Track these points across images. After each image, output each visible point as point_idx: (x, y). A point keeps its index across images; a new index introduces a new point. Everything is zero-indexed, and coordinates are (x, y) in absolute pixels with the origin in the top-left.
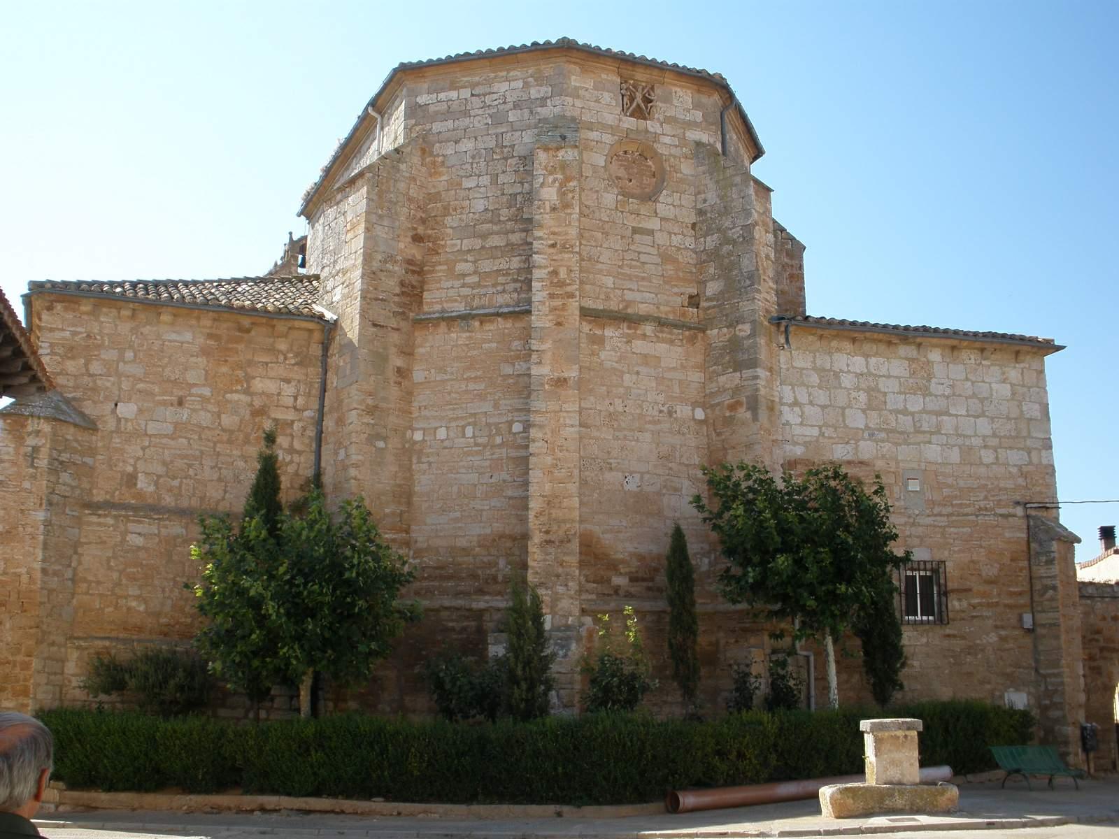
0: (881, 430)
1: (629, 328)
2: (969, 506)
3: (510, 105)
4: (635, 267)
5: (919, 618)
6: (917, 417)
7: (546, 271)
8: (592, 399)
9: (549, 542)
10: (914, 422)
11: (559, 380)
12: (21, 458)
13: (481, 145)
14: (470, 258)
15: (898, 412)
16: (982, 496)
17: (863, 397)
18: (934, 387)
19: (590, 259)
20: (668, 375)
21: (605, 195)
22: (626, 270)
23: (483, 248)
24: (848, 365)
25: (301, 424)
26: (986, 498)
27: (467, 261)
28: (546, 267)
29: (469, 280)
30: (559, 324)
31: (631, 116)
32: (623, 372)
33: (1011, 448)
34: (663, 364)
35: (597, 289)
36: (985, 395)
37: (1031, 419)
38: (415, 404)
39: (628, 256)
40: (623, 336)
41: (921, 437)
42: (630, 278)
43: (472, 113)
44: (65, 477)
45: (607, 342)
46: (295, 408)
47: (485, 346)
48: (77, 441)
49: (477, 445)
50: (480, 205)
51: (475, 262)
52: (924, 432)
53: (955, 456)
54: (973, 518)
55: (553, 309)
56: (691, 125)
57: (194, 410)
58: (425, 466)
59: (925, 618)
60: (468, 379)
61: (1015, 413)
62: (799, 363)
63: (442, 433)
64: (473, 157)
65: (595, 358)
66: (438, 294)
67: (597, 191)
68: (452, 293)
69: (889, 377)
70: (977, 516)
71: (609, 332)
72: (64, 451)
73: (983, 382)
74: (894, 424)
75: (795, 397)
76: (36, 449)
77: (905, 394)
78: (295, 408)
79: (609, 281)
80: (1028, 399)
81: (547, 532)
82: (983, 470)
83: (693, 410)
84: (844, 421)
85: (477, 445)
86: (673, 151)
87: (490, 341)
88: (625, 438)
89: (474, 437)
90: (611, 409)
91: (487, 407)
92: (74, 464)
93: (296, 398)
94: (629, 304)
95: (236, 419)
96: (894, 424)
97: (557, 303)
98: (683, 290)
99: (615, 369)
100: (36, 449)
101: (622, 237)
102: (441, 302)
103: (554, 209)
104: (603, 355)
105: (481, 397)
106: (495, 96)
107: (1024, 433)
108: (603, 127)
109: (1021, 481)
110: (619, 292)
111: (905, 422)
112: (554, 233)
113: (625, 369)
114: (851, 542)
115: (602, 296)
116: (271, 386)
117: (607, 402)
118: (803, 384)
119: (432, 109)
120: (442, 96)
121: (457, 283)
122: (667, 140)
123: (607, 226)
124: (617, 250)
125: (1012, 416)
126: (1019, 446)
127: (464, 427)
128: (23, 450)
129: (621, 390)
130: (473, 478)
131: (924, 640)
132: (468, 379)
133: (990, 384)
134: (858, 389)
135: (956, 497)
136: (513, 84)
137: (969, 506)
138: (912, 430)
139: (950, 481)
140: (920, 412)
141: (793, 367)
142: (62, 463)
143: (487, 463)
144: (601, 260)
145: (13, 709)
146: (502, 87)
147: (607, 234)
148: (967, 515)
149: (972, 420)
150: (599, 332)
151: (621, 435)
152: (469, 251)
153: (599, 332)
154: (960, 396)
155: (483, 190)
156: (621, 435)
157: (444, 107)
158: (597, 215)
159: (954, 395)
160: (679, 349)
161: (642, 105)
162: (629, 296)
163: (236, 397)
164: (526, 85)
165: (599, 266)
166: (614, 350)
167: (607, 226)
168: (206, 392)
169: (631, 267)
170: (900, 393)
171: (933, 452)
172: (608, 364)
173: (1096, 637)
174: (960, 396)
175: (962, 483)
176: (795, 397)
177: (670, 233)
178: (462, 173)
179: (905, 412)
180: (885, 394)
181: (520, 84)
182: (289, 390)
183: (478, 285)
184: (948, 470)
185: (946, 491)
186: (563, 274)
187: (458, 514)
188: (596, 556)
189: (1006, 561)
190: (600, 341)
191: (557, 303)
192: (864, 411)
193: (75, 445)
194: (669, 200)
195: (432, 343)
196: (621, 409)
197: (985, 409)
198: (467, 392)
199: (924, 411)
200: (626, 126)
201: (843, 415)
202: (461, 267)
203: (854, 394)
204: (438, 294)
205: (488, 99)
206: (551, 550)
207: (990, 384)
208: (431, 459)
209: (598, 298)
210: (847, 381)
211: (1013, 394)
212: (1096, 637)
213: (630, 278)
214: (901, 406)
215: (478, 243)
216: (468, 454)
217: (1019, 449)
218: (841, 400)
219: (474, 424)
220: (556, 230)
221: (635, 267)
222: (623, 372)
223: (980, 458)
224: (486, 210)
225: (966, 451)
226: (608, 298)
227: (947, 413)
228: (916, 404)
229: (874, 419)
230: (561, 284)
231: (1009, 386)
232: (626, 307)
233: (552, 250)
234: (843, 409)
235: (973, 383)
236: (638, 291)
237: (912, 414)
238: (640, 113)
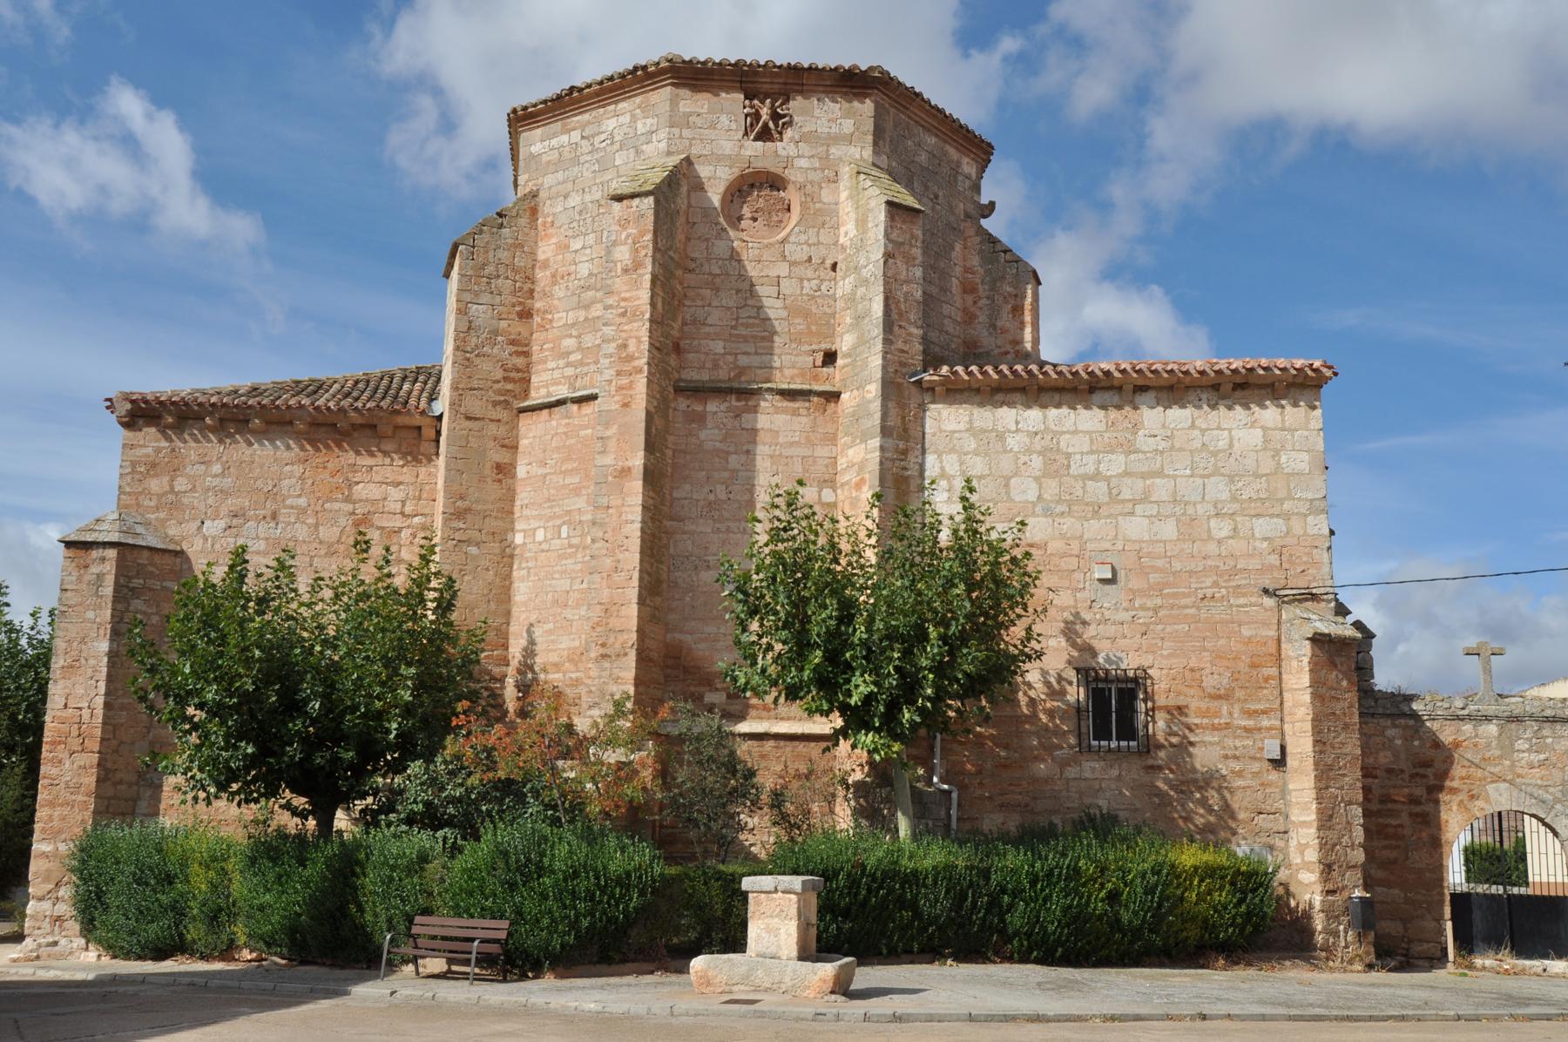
0: (1059, 501)
1: (738, 400)
2: (1185, 595)
3: (617, 146)
4: (753, 325)
5: (1114, 744)
6: (1114, 482)
7: (614, 345)
8: (688, 487)
9: (604, 656)
10: (1110, 490)
11: (623, 470)
12: (84, 587)
13: (588, 198)
14: (574, 333)
15: (1086, 477)
16: (1209, 582)
17: (1037, 462)
18: (1142, 441)
19: (694, 322)
20: (786, 452)
21: (717, 242)
22: (742, 331)
23: (586, 319)
24: (1017, 423)
25: (410, 531)
26: (1216, 584)
27: (571, 336)
28: (613, 340)
29: (572, 358)
30: (626, 405)
31: (755, 140)
32: (728, 453)
33: (1258, 516)
34: (781, 440)
35: (703, 357)
36: (1222, 444)
37: (1292, 474)
38: (518, 503)
39: (744, 313)
40: (729, 410)
41: (1118, 508)
42: (745, 339)
43: (582, 160)
44: (137, 604)
45: (709, 418)
46: (402, 513)
47: (583, 433)
48: (155, 565)
49: (570, 546)
50: (584, 269)
51: (579, 337)
52: (1123, 501)
53: (1169, 530)
54: (1192, 611)
55: (620, 388)
56: (836, 139)
57: (289, 524)
58: (524, 572)
59: (1123, 743)
60: (565, 473)
61: (1267, 466)
62: (950, 426)
63: (540, 535)
64: (580, 213)
65: (693, 440)
66: (545, 376)
67: (707, 240)
68: (557, 374)
69: (1076, 432)
70: (1198, 608)
71: (712, 406)
72: (138, 575)
73: (1219, 428)
74: (1080, 493)
75: (942, 468)
76: (100, 577)
77: (1097, 452)
78: (402, 513)
79: (718, 346)
80: (1289, 447)
81: (603, 645)
82: (1212, 548)
83: (820, 493)
84: (1008, 493)
85: (570, 546)
86: (812, 176)
87: (587, 427)
88: (728, 530)
89: (569, 537)
90: (712, 497)
91: (581, 503)
92: (151, 590)
93: (403, 503)
94: (742, 371)
95: (336, 530)
96: (1080, 493)
97: (624, 381)
98: (814, 347)
99: (719, 450)
100: (100, 577)
101: (738, 291)
102: (547, 386)
103: (626, 271)
104: (703, 435)
105: (576, 491)
106: (603, 137)
107: (1282, 494)
108: (718, 159)
109: (1273, 559)
110: (730, 358)
111: (1098, 490)
112: (625, 300)
113: (732, 449)
114: (819, 653)
115: (709, 365)
116: (373, 491)
117: (706, 490)
118: (952, 450)
119: (545, 158)
120: (554, 142)
121: (561, 363)
122: (803, 163)
123: (718, 280)
124: (729, 308)
125: (1263, 470)
126: (1271, 511)
127: (560, 527)
128: (87, 578)
129: (726, 474)
130: (564, 584)
131: (1115, 772)
132: (565, 473)
133: (1230, 430)
134: (1029, 451)
135: (1167, 585)
136: (621, 119)
137: (1185, 595)
138: (1107, 499)
139: (1160, 563)
140: (1119, 475)
141: (941, 431)
142: (132, 589)
143: (578, 567)
144: (709, 321)
145: (744, 875)
146: (610, 124)
147: (718, 290)
148: (1187, 607)
149: (1199, 481)
150: (699, 408)
151: (722, 527)
152: (573, 325)
153: (699, 408)
154: (1181, 450)
155: (588, 251)
156: (722, 527)
157: (554, 155)
158: (706, 268)
159: (1172, 448)
160: (804, 420)
161: (771, 125)
162: (743, 361)
163: (336, 506)
164: (634, 119)
165: (707, 329)
166: (718, 427)
167: (718, 280)
168: (302, 501)
169: (747, 326)
170: (1092, 452)
171: (1136, 527)
172: (709, 445)
173: (1421, 771)
174: (1181, 450)
175: (1177, 565)
176: (942, 468)
177: (802, 280)
178: (570, 233)
179: (1096, 476)
180: (1068, 456)
181: (626, 119)
182: (395, 494)
183: (581, 363)
184: (1159, 548)
185: (1154, 578)
186: (632, 348)
187: (551, 626)
188: (686, 670)
189: (1242, 666)
190: (701, 419)
191: (624, 381)
192: (1036, 479)
193: (151, 569)
194: (803, 238)
195: (532, 431)
196: (723, 496)
197: (1220, 464)
198: (564, 486)
199: (1126, 474)
200: (748, 153)
201: (1007, 485)
202: (569, 343)
203: (1023, 458)
204: (545, 376)
205: (597, 139)
206: (607, 665)
207: (1230, 430)
208: (530, 564)
209: (703, 367)
210: (1013, 442)
211: (1266, 441)
212: (1421, 771)
213: (745, 339)
214: (1091, 469)
215: (582, 315)
216: (561, 557)
217: (1272, 516)
218: (1006, 465)
219: (569, 523)
220: (627, 295)
221: (753, 325)
222: (728, 453)
223: (1209, 530)
224: (590, 275)
225: (1189, 526)
226: (716, 366)
227: (1160, 474)
228: (1115, 464)
229: (1052, 488)
230: (630, 358)
231: (1259, 432)
232: (739, 375)
233: (624, 320)
234: (1008, 479)
235: (1203, 431)
236: (756, 353)
237: (1108, 479)
238: (765, 135)
